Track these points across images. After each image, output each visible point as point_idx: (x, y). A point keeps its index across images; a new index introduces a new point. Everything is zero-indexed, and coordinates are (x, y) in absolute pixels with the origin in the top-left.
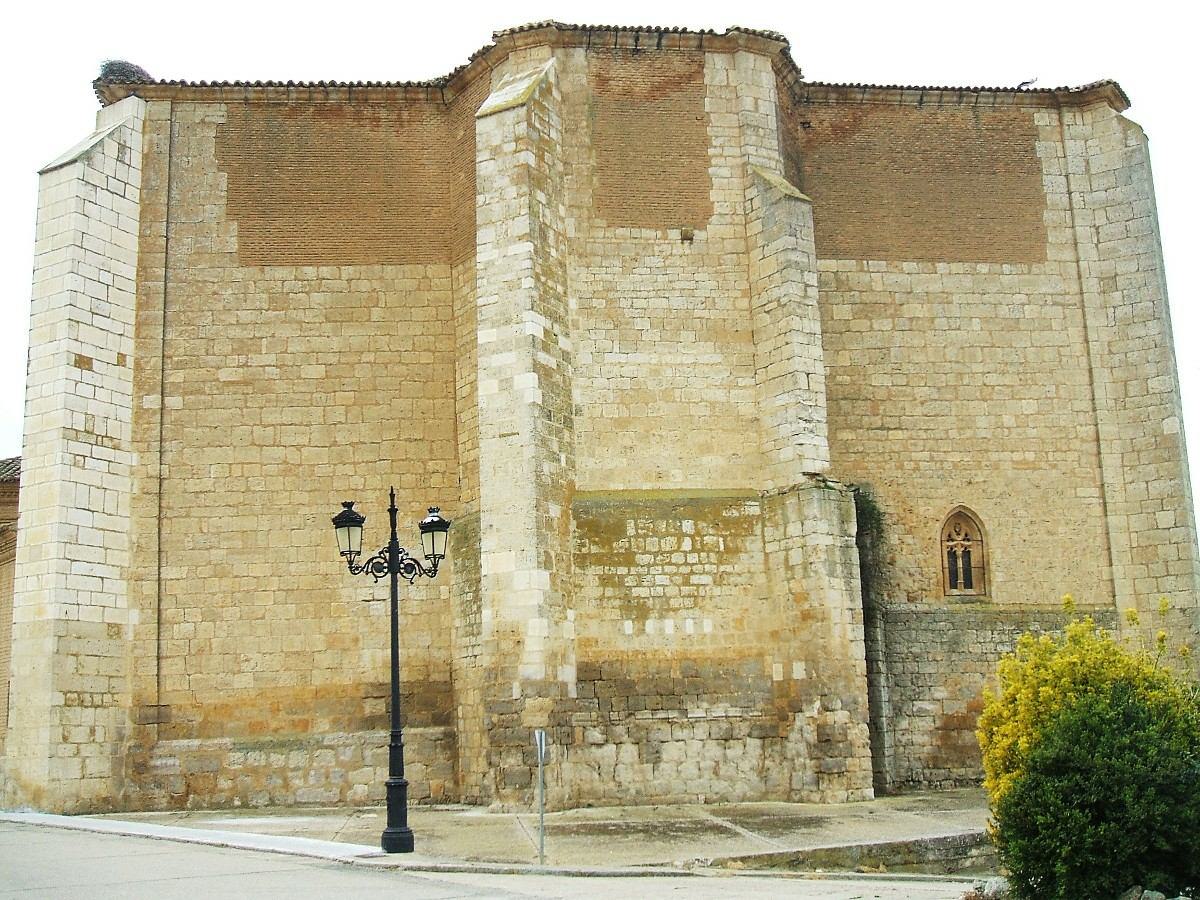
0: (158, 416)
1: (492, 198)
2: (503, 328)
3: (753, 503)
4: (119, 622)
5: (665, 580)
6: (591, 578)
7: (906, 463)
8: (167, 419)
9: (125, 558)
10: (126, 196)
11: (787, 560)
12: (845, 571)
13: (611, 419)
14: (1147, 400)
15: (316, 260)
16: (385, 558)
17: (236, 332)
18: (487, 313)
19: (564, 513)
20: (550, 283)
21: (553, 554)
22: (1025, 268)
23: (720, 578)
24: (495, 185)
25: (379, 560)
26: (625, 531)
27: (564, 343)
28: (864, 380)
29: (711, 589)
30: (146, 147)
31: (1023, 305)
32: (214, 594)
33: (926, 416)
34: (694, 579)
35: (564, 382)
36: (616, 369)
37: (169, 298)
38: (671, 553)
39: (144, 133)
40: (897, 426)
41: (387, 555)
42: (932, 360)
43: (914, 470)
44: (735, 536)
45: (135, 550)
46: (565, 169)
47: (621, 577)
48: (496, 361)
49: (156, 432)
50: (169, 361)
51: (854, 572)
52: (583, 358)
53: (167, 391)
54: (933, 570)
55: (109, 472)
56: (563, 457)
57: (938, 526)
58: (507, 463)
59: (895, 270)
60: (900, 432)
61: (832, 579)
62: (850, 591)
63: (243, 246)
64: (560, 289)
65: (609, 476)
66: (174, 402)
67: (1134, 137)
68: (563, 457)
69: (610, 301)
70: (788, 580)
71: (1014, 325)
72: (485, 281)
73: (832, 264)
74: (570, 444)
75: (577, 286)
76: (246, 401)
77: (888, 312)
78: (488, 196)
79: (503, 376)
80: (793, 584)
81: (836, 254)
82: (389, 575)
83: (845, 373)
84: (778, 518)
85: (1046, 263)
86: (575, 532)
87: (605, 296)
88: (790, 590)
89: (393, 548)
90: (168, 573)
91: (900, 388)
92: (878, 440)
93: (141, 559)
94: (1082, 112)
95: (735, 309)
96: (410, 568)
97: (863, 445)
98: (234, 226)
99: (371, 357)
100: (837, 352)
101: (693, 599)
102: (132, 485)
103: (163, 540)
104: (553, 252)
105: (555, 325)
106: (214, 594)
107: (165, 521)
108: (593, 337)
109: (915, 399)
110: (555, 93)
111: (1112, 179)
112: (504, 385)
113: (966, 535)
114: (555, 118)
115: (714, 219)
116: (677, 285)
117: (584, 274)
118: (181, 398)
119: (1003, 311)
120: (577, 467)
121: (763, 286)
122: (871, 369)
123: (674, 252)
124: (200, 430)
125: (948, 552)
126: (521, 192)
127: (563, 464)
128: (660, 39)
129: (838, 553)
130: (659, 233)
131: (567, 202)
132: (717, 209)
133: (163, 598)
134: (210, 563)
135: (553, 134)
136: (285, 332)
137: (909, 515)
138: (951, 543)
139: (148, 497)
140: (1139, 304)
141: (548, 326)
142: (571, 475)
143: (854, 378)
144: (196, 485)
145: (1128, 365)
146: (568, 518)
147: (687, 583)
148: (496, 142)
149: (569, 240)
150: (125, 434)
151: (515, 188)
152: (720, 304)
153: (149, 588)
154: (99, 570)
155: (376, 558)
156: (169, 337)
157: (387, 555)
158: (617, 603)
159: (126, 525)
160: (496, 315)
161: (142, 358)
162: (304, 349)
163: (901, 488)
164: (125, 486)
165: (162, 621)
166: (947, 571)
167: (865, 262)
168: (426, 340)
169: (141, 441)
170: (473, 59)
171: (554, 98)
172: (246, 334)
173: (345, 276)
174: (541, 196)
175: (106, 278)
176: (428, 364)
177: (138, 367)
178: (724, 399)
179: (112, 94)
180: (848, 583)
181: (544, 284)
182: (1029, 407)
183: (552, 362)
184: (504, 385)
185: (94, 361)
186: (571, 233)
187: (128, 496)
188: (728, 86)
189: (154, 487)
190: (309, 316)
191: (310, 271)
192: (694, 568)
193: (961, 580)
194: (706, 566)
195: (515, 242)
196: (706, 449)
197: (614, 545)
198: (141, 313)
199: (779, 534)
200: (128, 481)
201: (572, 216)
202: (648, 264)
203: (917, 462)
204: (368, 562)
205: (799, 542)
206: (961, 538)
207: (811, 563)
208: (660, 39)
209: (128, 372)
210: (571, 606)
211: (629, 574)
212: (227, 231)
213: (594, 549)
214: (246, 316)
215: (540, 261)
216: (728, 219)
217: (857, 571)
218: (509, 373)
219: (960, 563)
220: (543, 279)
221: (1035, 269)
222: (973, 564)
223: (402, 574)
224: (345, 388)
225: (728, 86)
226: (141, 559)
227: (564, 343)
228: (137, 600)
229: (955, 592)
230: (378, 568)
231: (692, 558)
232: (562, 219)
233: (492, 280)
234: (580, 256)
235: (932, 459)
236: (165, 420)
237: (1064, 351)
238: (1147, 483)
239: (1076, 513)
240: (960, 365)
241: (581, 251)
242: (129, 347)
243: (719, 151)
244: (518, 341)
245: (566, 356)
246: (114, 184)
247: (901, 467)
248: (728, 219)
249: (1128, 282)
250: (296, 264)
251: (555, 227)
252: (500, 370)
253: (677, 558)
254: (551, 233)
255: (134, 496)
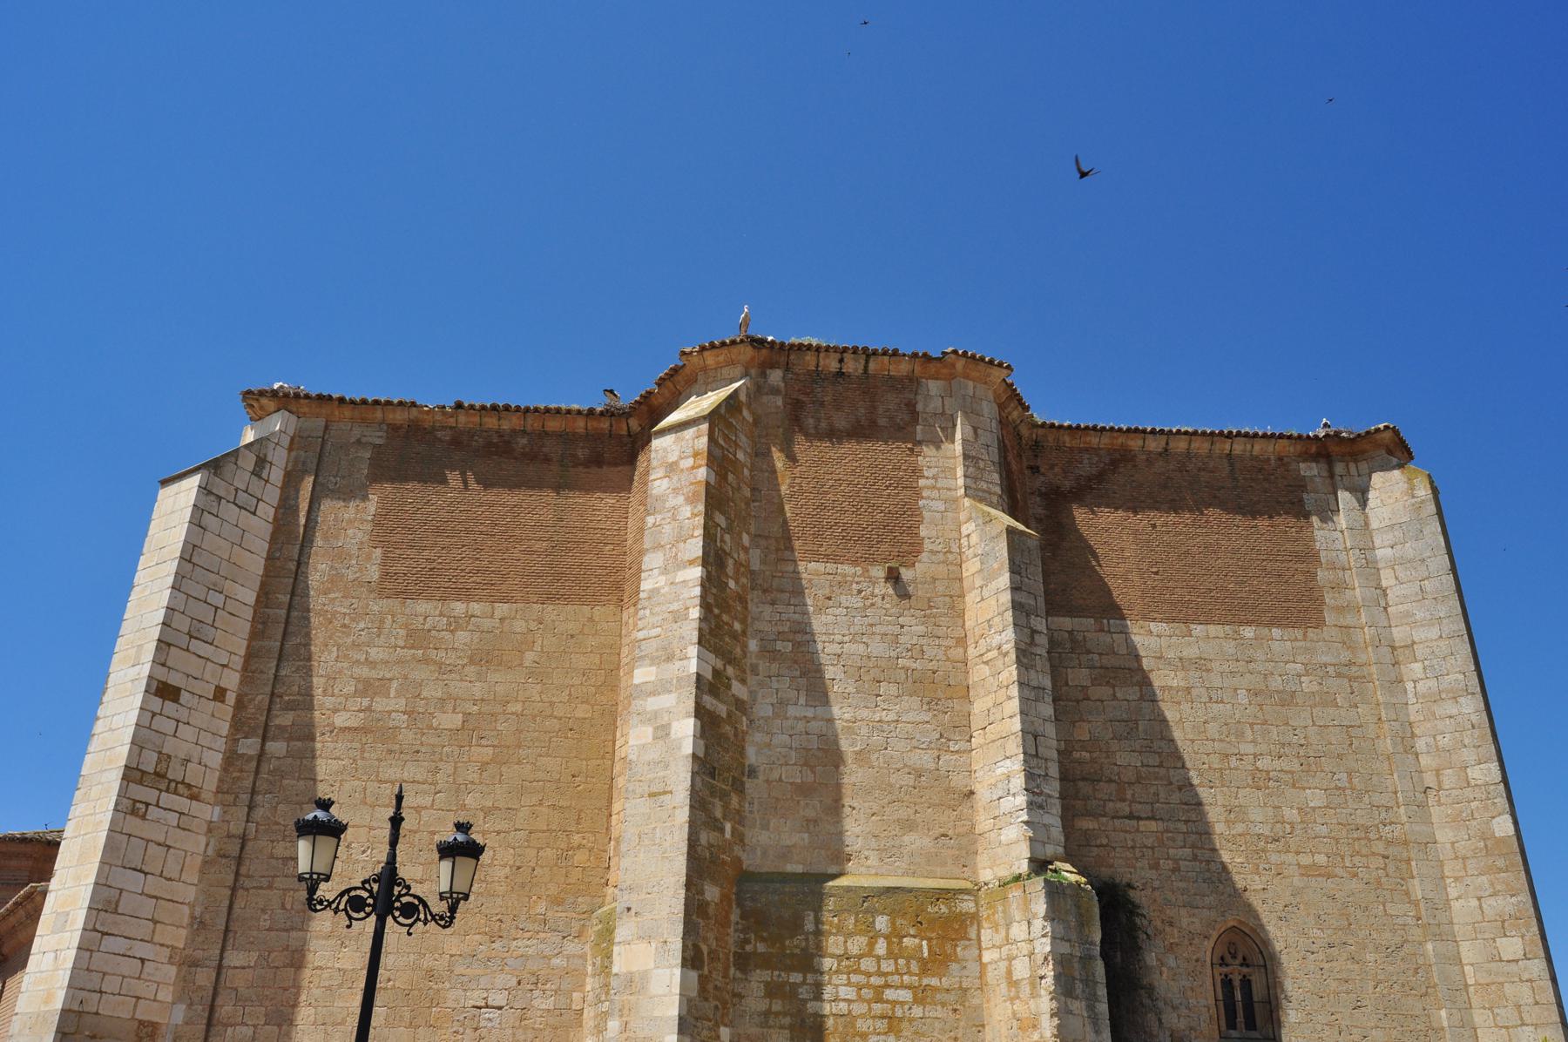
0: (254, 764)
1: (664, 519)
2: (665, 666)
3: (966, 897)
4: (155, 1019)
5: (852, 995)
6: (754, 985)
7: (1161, 862)
8: (265, 767)
9: (178, 937)
10: (258, 513)
11: (1009, 972)
12: (1087, 990)
13: (791, 784)
14: (1468, 793)
15: (466, 595)
16: (370, 891)
17: (365, 672)
18: (649, 648)
19: (725, 897)
20: (725, 618)
21: (705, 949)
22: (1299, 633)
23: (922, 995)
24: (667, 505)
25: (358, 892)
26: (802, 926)
27: (738, 689)
28: (1108, 757)
29: (910, 1008)
30: (290, 465)
31: (1299, 676)
32: (286, 989)
33: (1186, 804)
34: (889, 994)
35: (736, 735)
36: (801, 726)
37: (291, 629)
38: (860, 957)
39: (290, 449)
40: (1150, 815)
41: (375, 887)
42: (1191, 737)
43: (1173, 871)
44: (943, 938)
45: (195, 926)
46: (753, 495)
47: (795, 986)
48: (652, 704)
49: (248, 783)
50: (278, 700)
51: (1099, 993)
52: (763, 709)
53: (270, 734)
54: (1203, 1002)
55: (178, 827)
56: (728, 827)
57: (1209, 944)
58: (654, 828)
59: (1142, 631)
60: (1153, 823)
61: (1069, 1001)
62: (1094, 1019)
63: (385, 575)
64: (737, 626)
65: (786, 853)
66: (276, 747)
67: (1422, 487)
68: (728, 827)
69: (797, 645)
70: (1012, 1000)
71: (1288, 699)
72: (647, 612)
73: (1066, 623)
74: (738, 812)
75: (758, 625)
76: (363, 751)
77: (1134, 680)
78: (659, 517)
79: (660, 722)
80: (1018, 1006)
81: (1072, 612)
82: (373, 918)
83: (1084, 748)
84: (999, 917)
85: (1325, 628)
86: (737, 923)
87: (791, 638)
88: (1014, 1014)
89: (389, 875)
90: (234, 958)
91: (1151, 769)
92: (1126, 832)
93: (200, 939)
94: (1356, 461)
95: (948, 659)
96: (409, 911)
97: (1107, 837)
98: (379, 551)
99: (518, 708)
100: (1073, 723)
101: (885, 1021)
102: (207, 845)
103: (234, 916)
104: (732, 584)
105: (728, 667)
106: (286, 989)
107: (240, 892)
108: (775, 685)
109: (1171, 783)
110: (745, 413)
111: (1398, 533)
112: (660, 733)
113: (1244, 959)
114: (743, 438)
115: (924, 556)
116: (878, 629)
117: (767, 610)
118: (286, 744)
119: (1276, 683)
120: (746, 841)
121: (981, 633)
122: (1114, 745)
123: (876, 591)
124: (302, 782)
125: (1222, 980)
126: (696, 511)
127: (728, 835)
128: (867, 362)
129: (1076, 965)
130: (859, 570)
131: (752, 529)
132: (927, 545)
133: (221, 990)
134: (287, 948)
135: (740, 456)
136: (420, 673)
137: (1168, 929)
138: (1225, 969)
139: (224, 861)
140: (1446, 677)
141: (719, 664)
142: (737, 850)
143: (1095, 755)
144: (286, 848)
145: (1438, 750)
146: (730, 906)
147: (879, 999)
148: (672, 458)
149: (752, 573)
150: (210, 783)
151: (688, 508)
152: (929, 652)
153: (204, 977)
154: (142, 950)
155: (355, 889)
156: (283, 673)
157: (375, 887)
158: (787, 1021)
159: (190, 894)
160: (657, 650)
161: (246, 695)
162: (439, 694)
163: (1157, 894)
164: (197, 845)
165: (215, 1022)
166: (1221, 1004)
167: (1105, 621)
168: (585, 690)
169: (227, 793)
170: (661, 382)
171: (744, 418)
172: (373, 674)
173: (498, 614)
174: (721, 519)
175: (217, 599)
176: (585, 719)
177: (240, 704)
178: (932, 766)
179: (261, 408)
180: (1091, 1008)
181: (718, 617)
182: (1315, 798)
183: (722, 710)
184: (660, 733)
185: (183, 692)
186: (756, 565)
187: (199, 859)
188: (943, 413)
189: (233, 848)
190: (451, 658)
191: (459, 607)
192: (890, 978)
193: (1240, 1019)
194: (905, 977)
195: (685, 568)
196: (909, 826)
197: (787, 942)
198: (254, 643)
199: (999, 938)
200: (203, 840)
201: (757, 547)
202: (845, 604)
203: (1176, 861)
204: (342, 895)
205: (1025, 948)
206: (1237, 962)
207: (1041, 978)
208: (867, 362)
209: (227, 710)
210: (726, 1020)
211: (804, 983)
212: (369, 558)
213: (761, 948)
214: (375, 653)
215: (714, 591)
216: (941, 557)
217: (1102, 992)
218: (666, 719)
219: (1238, 995)
220: (716, 611)
221: (1311, 633)
222: (1255, 999)
223: (395, 918)
224: (483, 742)
225: (943, 413)
226: (200, 939)
227: (738, 689)
228: (185, 989)
229: (1234, 1033)
230: (357, 904)
231: (887, 966)
232: (746, 550)
233: (657, 609)
234: (765, 591)
235: (1195, 858)
236: (261, 769)
237: (1354, 732)
238: (1479, 899)
239: (1388, 935)
240: (1224, 745)
241: (765, 586)
242: (231, 681)
243: (930, 482)
244: (679, 679)
245: (740, 704)
246: (242, 497)
247: (1155, 866)
248: (941, 557)
249: (1428, 650)
250: (443, 599)
251: (736, 556)
252: (656, 714)
253: (868, 964)
254: (730, 562)
255: (207, 859)
